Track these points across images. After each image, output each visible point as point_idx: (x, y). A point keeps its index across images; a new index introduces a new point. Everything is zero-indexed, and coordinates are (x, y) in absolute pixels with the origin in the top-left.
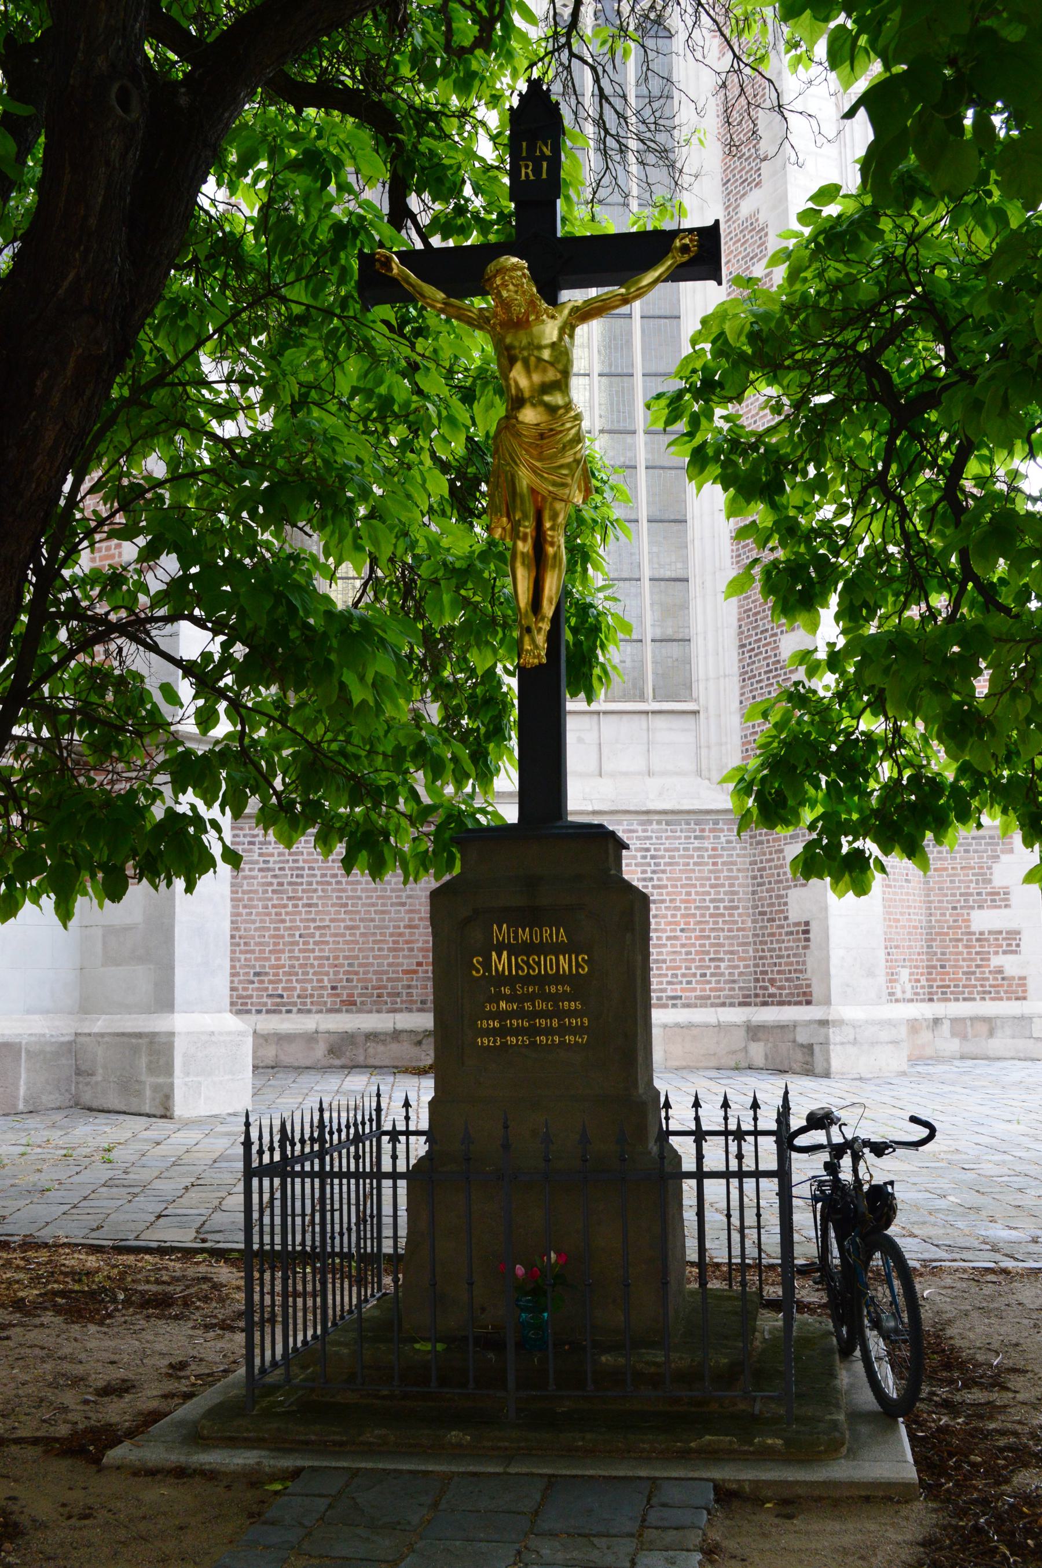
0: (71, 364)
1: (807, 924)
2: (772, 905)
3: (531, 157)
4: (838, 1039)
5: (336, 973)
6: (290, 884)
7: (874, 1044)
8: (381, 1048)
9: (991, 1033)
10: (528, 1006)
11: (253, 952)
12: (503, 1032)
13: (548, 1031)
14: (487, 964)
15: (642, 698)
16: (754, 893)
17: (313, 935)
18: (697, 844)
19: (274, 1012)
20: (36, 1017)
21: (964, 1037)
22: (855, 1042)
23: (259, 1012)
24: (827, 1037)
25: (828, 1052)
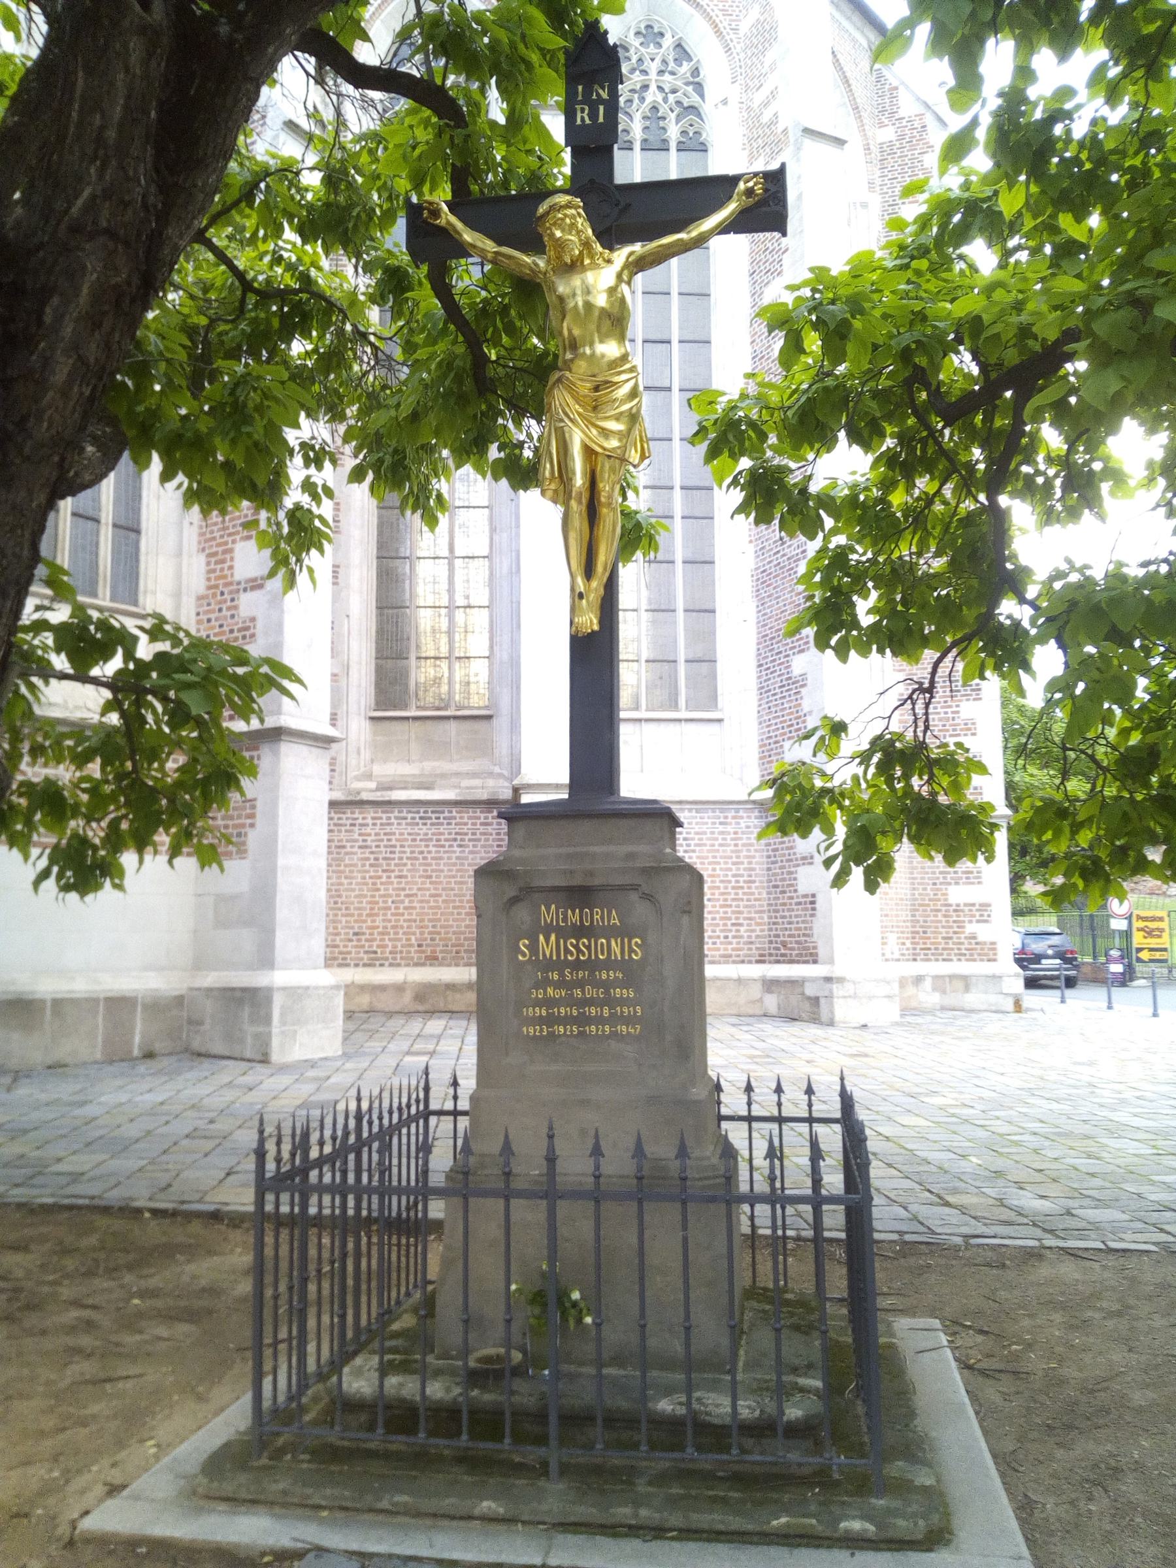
0: (85, 290)
1: (813, 896)
2: (783, 880)
3: (587, 100)
4: (841, 993)
5: (422, 933)
6: (385, 859)
7: (870, 998)
8: (458, 996)
9: (967, 989)
10: (578, 993)
11: (352, 915)
12: (550, 1020)
13: (600, 1020)
14: (534, 947)
15: (675, 706)
16: (769, 869)
17: (402, 902)
18: (721, 828)
19: (369, 965)
20: (152, 974)
21: (944, 992)
22: (855, 996)
23: (357, 965)
24: (831, 991)
25: (832, 1004)
